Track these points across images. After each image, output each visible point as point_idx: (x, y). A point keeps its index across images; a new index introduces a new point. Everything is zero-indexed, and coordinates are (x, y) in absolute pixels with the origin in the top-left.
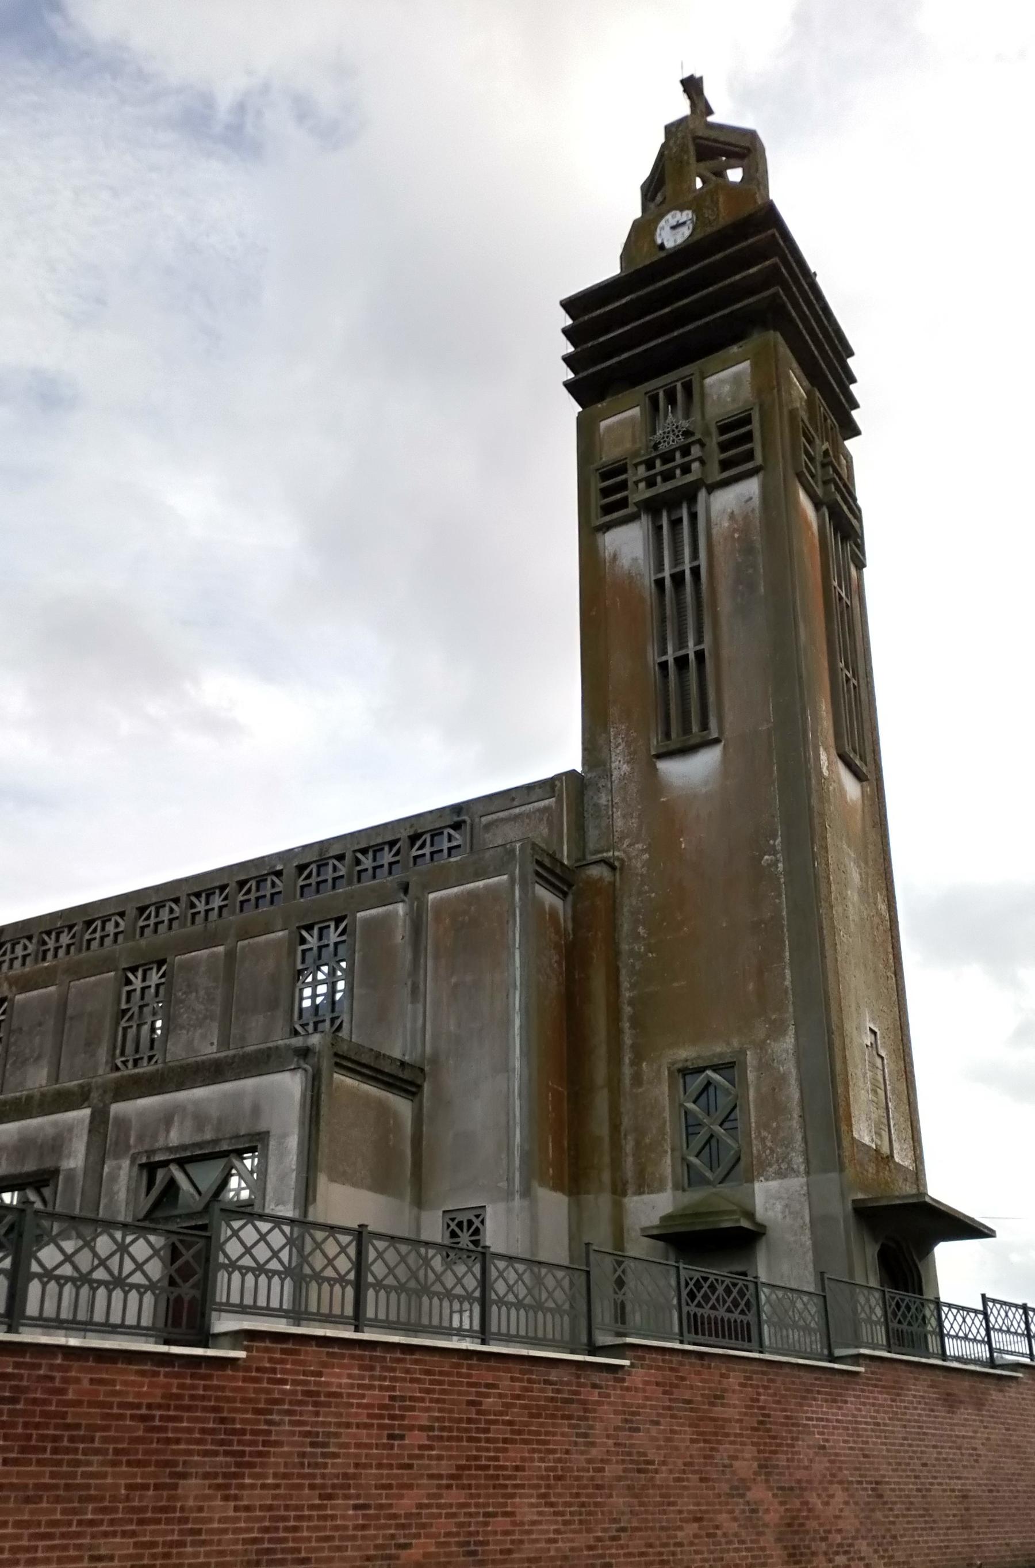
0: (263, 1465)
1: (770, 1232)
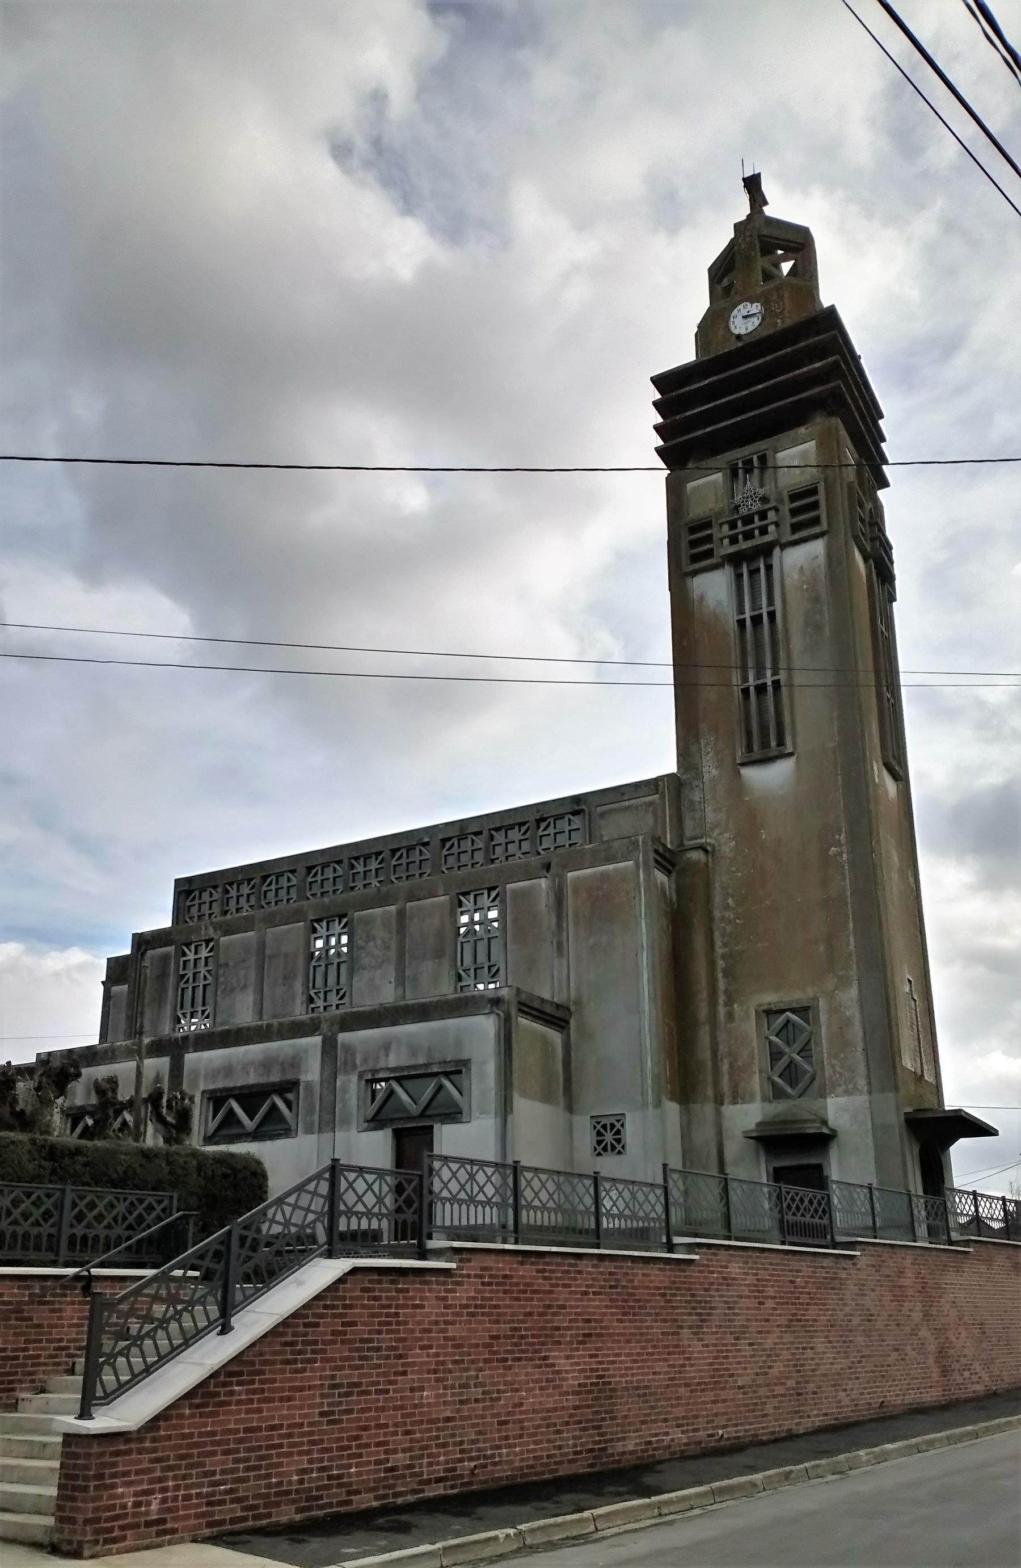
0: (710, 1321)
1: (841, 1136)
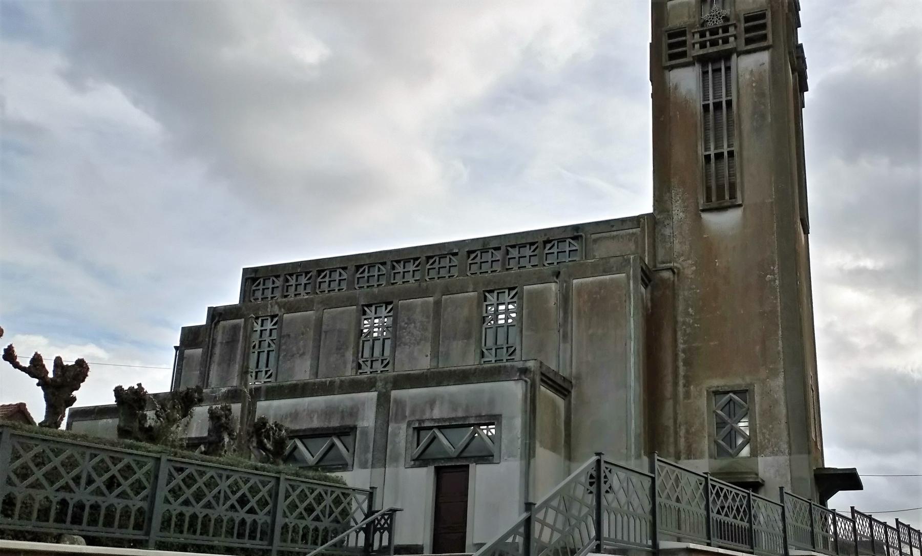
1: (767, 484)
